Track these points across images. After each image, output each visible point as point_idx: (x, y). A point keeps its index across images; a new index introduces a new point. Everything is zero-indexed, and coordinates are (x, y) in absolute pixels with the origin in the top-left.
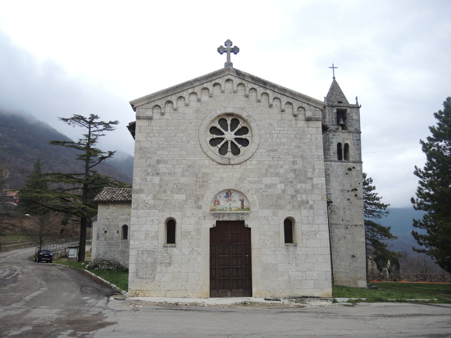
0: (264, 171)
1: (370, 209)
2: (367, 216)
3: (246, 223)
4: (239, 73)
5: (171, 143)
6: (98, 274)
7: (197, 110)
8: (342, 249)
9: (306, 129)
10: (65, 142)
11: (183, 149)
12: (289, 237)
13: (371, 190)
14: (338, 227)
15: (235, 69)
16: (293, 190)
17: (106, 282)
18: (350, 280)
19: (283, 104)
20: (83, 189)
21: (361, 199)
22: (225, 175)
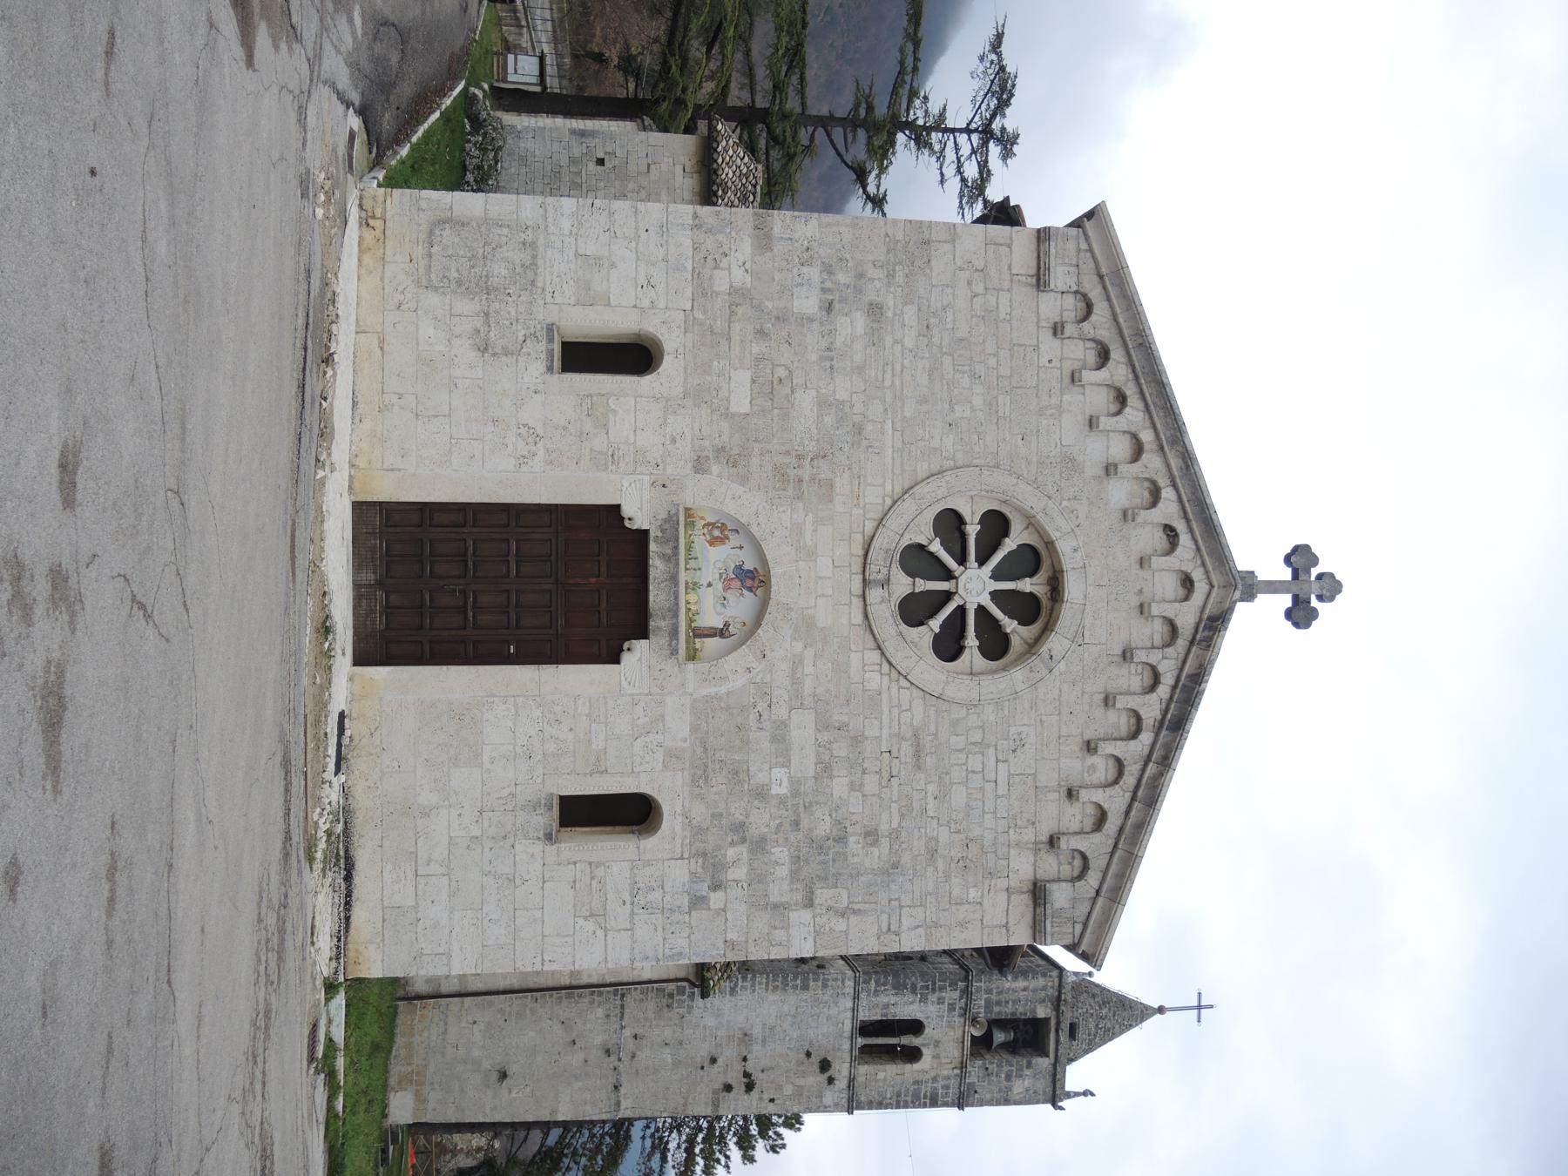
0: (839, 717)
1: (672, 1146)
2: (649, 1132)
3: (640, 646)
4: (1214, 624)
5: (947, 360)
6: (446, 118)
7: (1073, 460)
8: (532, 1034)
9: (1002, 883)
10: (917, 44)
12: (584, 813)
13: (741, 1148)
14: (613, 1019)
15: (1230, 610)
17: (420, 133)
18: (416, 1061)
19: (1100, 796)
20: (752, 107)
21: (716, 1105)
22: (824, 565)
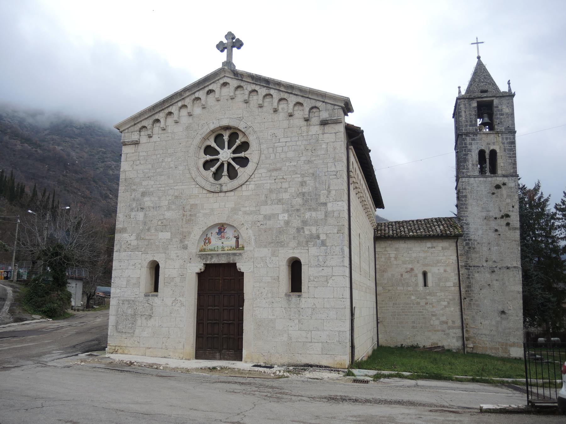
0: (263, 198)
3: (238, 266)
4: (237, 75)
5: (158, 170)
8: (485, 301)
9: (321, 136)
11: (171, 177)
12: (296, 285)
16: (299, 221)
18: (497, 346)
22: (216, 206)
